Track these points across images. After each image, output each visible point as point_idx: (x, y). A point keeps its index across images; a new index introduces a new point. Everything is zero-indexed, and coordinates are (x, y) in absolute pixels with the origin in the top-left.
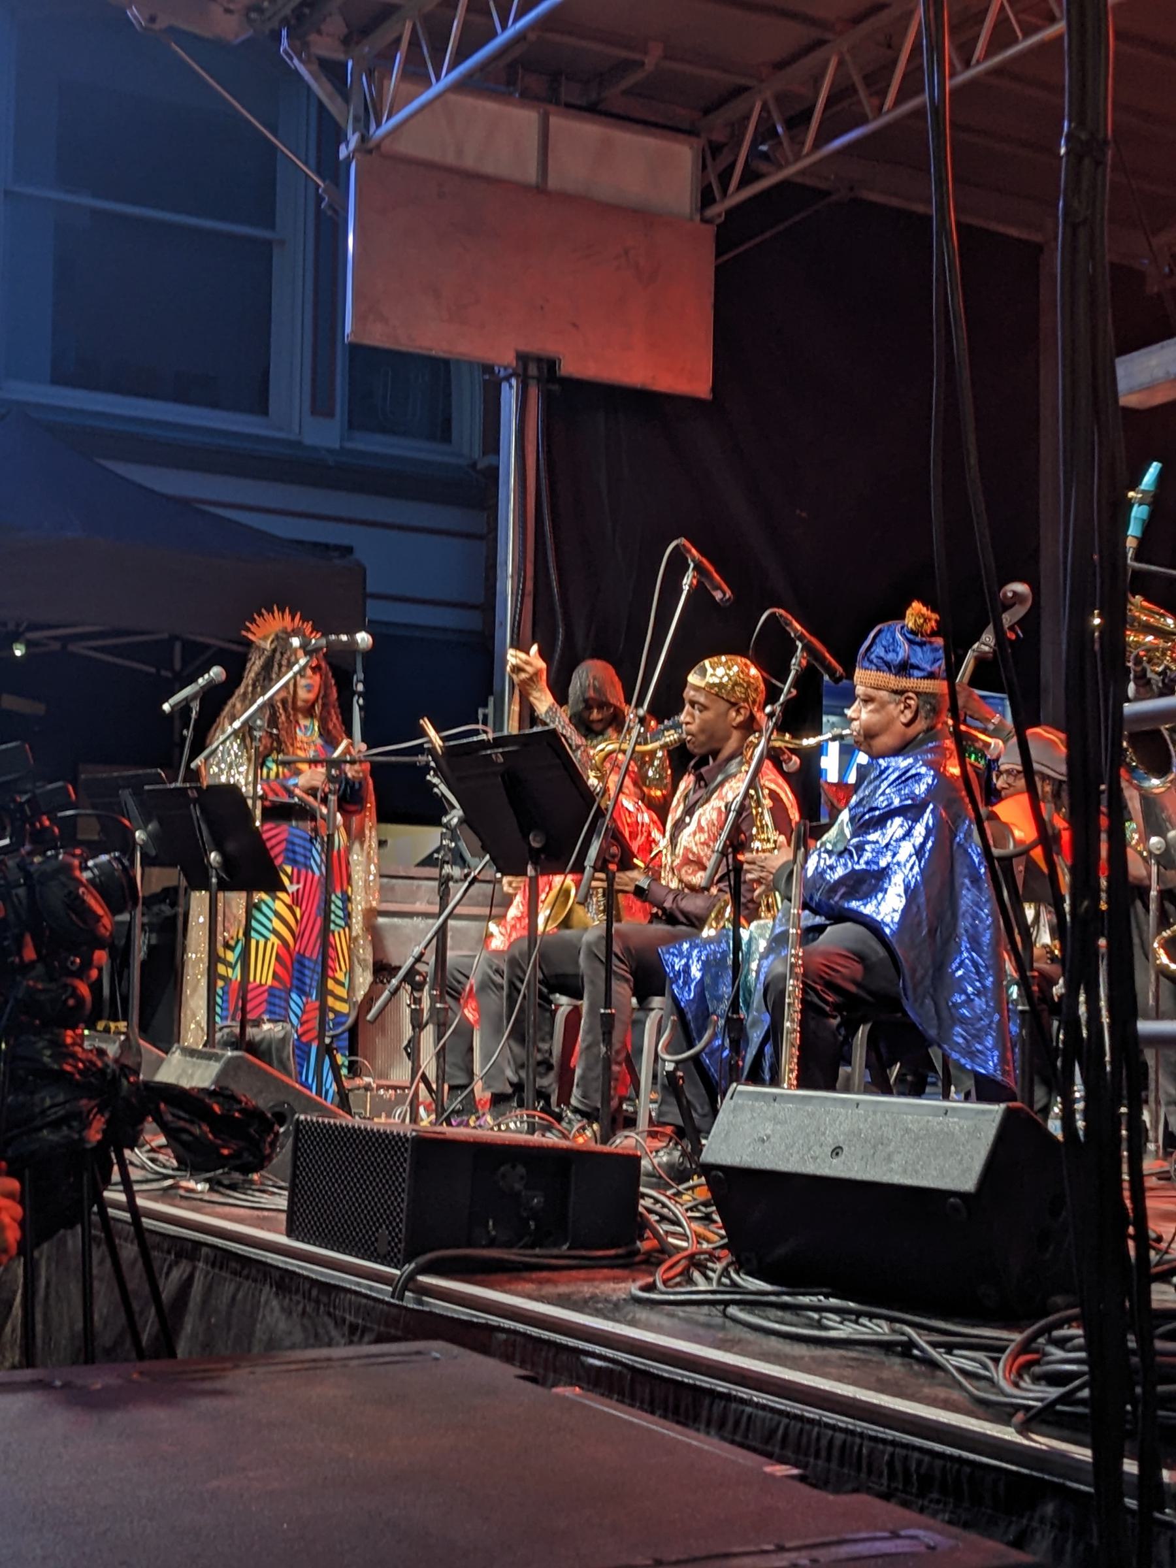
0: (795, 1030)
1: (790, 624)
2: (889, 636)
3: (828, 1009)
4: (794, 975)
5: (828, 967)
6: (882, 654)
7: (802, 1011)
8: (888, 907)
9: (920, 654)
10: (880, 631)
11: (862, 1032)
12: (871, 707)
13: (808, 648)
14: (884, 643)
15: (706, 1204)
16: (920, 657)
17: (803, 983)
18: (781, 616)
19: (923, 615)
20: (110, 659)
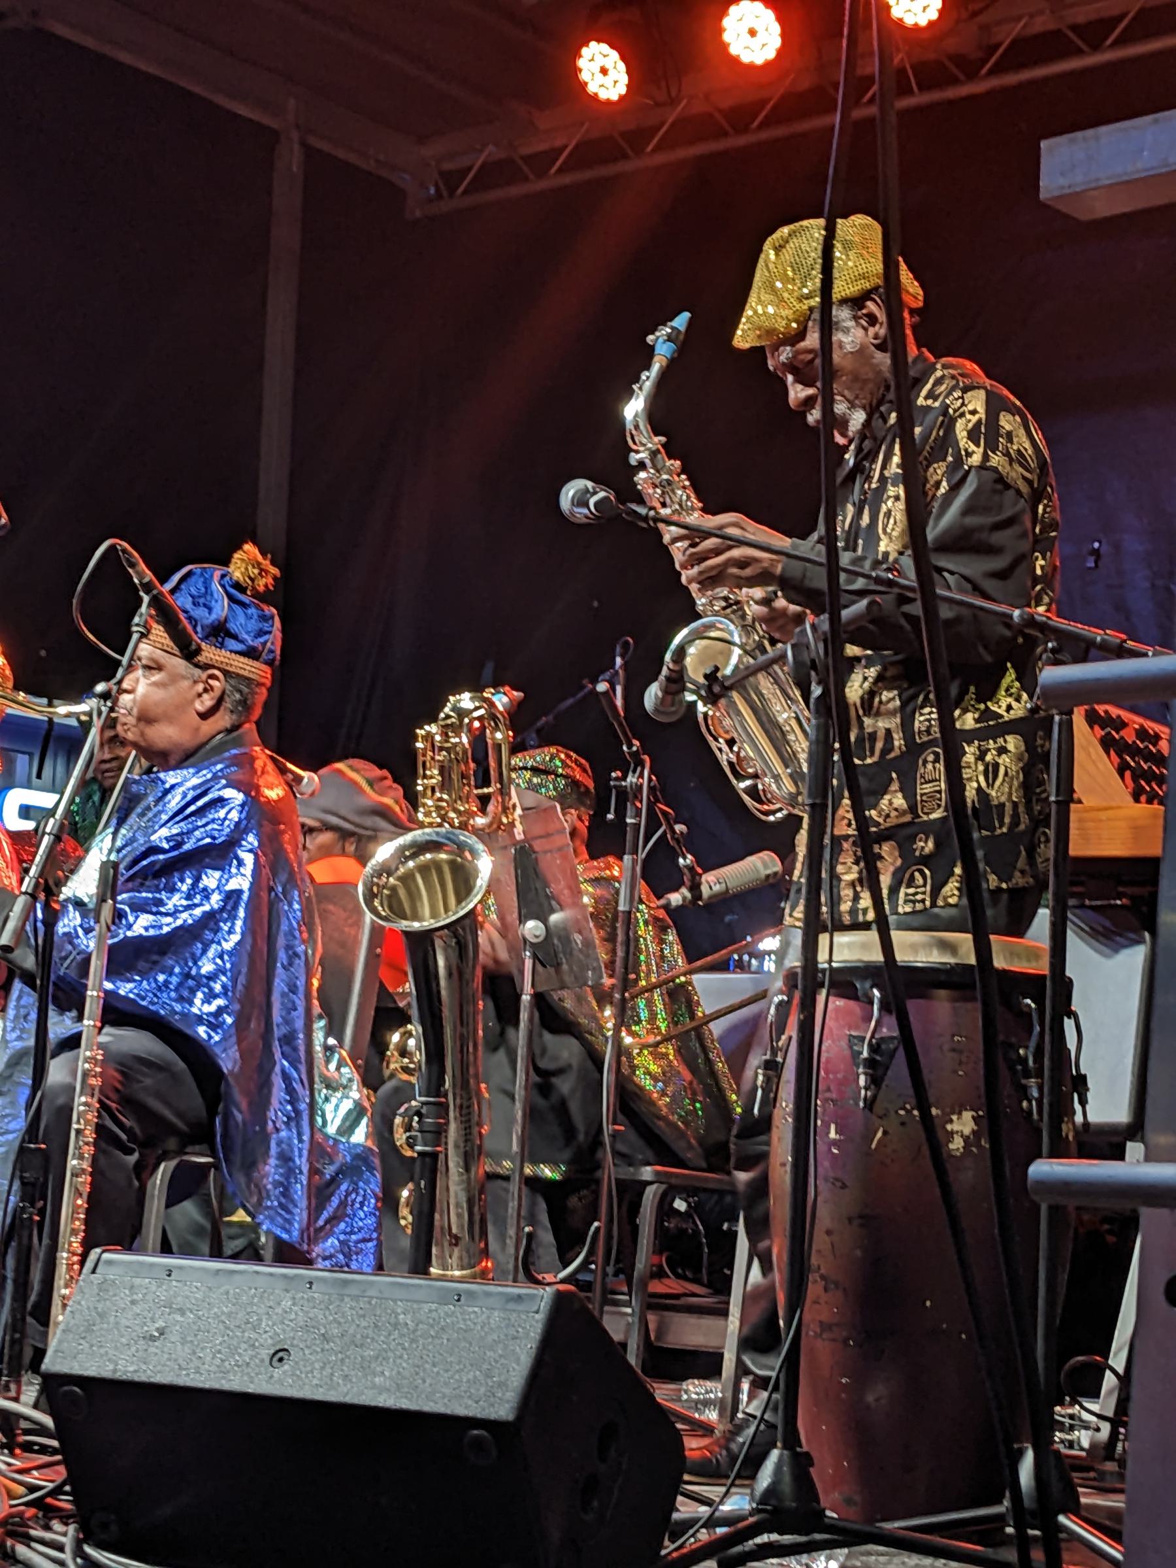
0: (83, 1171)
1: (133, 565)
2: (200, 586)
4: (87, 1089)
6: (189, 606)
9: (242, 619)
10: (189, 574)
12: (157, 677)
14: (193, 591)
16: (243, 623)
17: (100, 1101)
18: (124, 551)
19: (259, 564)
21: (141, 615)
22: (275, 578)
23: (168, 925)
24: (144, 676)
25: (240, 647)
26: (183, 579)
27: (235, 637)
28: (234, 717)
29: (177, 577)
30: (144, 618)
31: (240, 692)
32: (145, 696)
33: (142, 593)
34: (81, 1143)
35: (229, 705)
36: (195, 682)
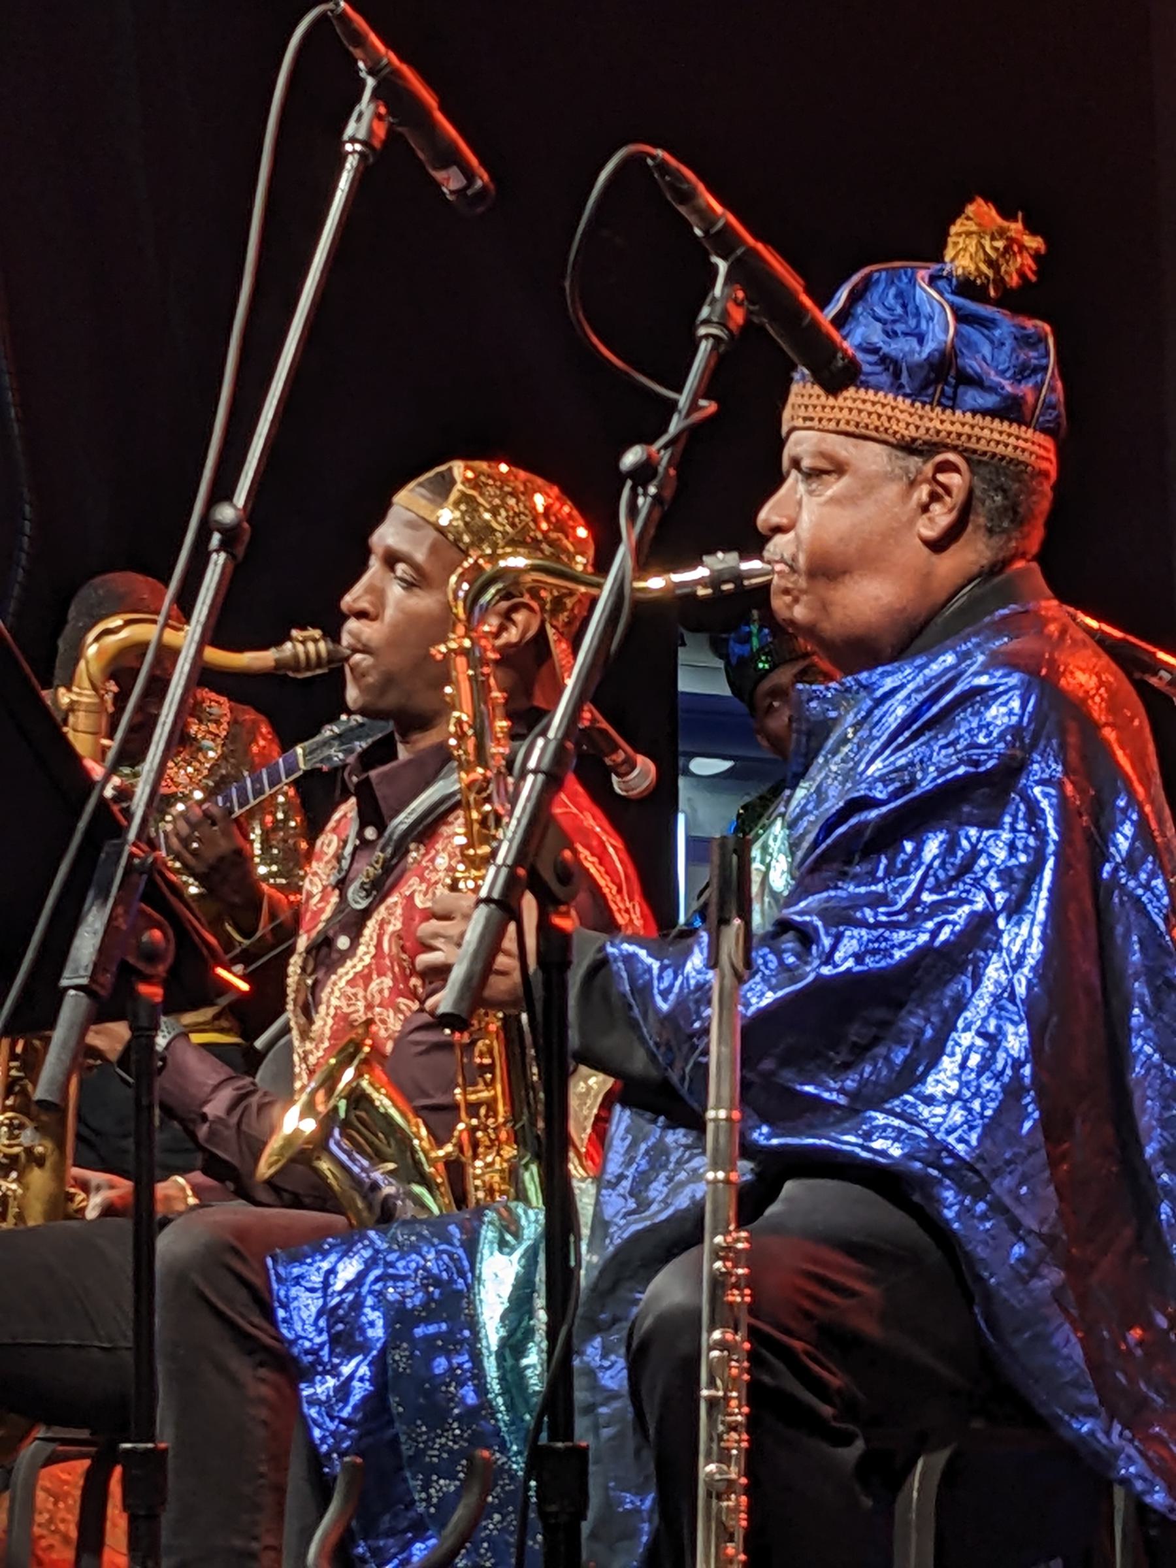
1: (687, 197)
3: (827, 1410)
4: (722, 1315)
5: (822, 1281)
6: (877, 337)
7: (753, 1425)
8: (956, 1086)
11: (921, 1481)
12: (836, 487)
13: (747, 273)
15: (20, 1217)
17: (754, 1334)
18: (662, 166)
20: (899, 802)
21: (714, 300)
22: (1037, 256)
23: (905, 944)
24: (811, 493)
25: (990, 400)
26: (856, 296)
27: (977, 382)
28: (997, 541)
29: (843, 294)
30: (719, 307)
31: (1004, 491)
32: (818, 525)
33: (715, 259)
34: (721, 1428)
35: (982, 520)
36: (913, 484)
